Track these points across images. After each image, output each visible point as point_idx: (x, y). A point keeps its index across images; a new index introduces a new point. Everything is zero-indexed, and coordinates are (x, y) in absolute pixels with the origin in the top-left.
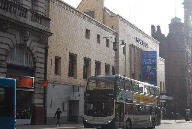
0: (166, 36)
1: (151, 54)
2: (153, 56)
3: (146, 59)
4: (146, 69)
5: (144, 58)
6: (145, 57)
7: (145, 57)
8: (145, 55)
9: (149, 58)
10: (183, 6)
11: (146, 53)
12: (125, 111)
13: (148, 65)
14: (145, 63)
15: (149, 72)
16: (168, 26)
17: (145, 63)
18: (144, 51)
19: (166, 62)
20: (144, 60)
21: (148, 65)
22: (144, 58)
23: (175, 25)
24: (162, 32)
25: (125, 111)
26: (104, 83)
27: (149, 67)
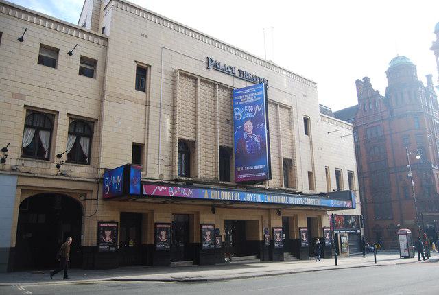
0: (383, 93)
1: (251, 93)
2: (257, 97)
3: (242, 106)
4: (242, 131)
5: (238, 106)
6: (240, 103)
7: (240, 103)
8: (241, 97)
9: (249, 104)
10: (432, 52)
11: (242, 92)
12: (118, 244)
13: (246, 120)
14: (239, 116)
15: (249, 138)
16: (385, 75)
17: (239, 116)
18: (238, 90)
19: (355, 130)
20: (237, 111)
21: (246, 120)
22: (238, 106)
23: (400, 71)
24: (373, 87)
25: (118, 244)
26: (132, 191)
27: (249, 126)
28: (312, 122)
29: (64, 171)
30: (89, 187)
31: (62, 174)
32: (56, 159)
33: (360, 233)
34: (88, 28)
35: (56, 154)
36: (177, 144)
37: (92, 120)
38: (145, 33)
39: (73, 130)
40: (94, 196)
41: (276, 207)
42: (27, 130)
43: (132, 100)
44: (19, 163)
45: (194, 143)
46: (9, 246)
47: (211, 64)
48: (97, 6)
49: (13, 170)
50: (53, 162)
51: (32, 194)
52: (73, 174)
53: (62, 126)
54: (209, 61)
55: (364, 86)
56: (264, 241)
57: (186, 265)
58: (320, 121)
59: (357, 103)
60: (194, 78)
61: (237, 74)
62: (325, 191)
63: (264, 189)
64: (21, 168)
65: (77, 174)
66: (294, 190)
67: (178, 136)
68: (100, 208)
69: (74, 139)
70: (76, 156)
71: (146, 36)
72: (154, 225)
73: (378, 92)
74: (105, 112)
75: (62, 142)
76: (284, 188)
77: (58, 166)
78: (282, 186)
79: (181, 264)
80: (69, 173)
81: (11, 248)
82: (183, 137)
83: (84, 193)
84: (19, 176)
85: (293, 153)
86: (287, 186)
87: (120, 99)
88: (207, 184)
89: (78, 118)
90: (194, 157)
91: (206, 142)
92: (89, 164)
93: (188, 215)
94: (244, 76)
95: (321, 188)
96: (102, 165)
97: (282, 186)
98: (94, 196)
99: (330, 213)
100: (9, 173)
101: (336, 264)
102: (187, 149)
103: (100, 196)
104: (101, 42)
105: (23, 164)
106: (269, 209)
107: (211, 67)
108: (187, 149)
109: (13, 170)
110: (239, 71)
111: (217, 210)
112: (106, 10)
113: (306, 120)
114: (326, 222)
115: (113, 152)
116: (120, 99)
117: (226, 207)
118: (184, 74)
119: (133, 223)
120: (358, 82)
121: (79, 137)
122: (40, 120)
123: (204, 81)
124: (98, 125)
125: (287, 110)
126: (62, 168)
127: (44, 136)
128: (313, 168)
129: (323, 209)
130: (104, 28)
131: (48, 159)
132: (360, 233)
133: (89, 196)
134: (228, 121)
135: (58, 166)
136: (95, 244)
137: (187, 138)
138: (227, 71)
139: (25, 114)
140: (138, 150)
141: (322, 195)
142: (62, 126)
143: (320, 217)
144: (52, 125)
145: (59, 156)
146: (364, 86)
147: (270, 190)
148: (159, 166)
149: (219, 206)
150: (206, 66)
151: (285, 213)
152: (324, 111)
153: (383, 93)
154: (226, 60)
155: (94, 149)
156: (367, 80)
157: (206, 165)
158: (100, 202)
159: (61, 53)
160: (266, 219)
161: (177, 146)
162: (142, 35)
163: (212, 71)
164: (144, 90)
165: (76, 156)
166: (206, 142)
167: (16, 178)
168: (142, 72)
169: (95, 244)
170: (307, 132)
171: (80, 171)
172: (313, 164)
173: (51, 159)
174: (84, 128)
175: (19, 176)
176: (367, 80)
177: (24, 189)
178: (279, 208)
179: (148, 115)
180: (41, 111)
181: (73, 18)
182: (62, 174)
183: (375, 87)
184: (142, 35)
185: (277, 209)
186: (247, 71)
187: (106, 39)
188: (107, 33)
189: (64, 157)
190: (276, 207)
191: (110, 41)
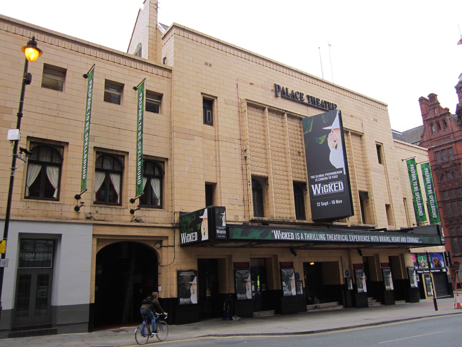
16: (455, 90)
28: (385, 150)
29: (139, 217)
30: (164, 233)
31: (137, 221)
32: (130, 204)
33: (446, 273)
34: (145, 56)
35: (129, 199)
36: (251, 181)
37: (162, 160)
38: (209, 62)
39: (101, 166)
40: (170, 242)
41: (356, 246)
42: (31, 166)
43: (202, 135)
44: (93, 210)
45: (266, 179)
46: (88, 302)
47: (280, 92)
48: (153, 34)
49: (88, 218)
50: (127, 208)
51: (108, 244)
52: (148, 219)
53: (132, 167)
54: (277, 88)
55: (429, 104)
56: (346, 285)
57: (267, 315)
58: (394, 148)
59: (421, 123)
60: (260, 107)
61: (306, 101)
62: (406, 226)
63: (346, 227)
64: (95, 216)
65: (151, 220)
66: (374, 226)
67: (250, 173)
68: (177, 255)
69: (102, 177)
70: (147, 200)
71: (210, 65)
72: (242, 271)
73: (447, 110)
74: (175, 151)
75: (131, 181)
76: (362, 225)
77: (132, 212)
78: (360, 222)
79: (262, 314)
80: (144, 219)
81: (91, 305)
82: (255, 173)
83: (160, 240)
84: (94, 224)
85: (368, 185)
86: (364, 222)
87: (189, 135)
88: (283, 225)
89: (148, 158)
90: (267, 194)
91: (278, 177)
92: (161, 207)
93: (265, 259)
94: (313, 102)
95: (400, 222)
96: (177, 209)
97: (360, 222)
98: (170, 242)
99: (413, 250)
100: (84, 221)
101: (436, 309)
102: (259, 185)
103: (177, 242)
104: (166, 74)
105: (97, 212)
106: (348, 249)
107: (279, 95)
108: (259, 185)
109: (88, 218)
110: (308, 96)
111: (298, 252)
112: (165, 40)
113: (379, 147)
114: (410, 262)
115: (185, 196)
116: (189, 135)
117: (305, 248)
118: (251, 105)
119: (208, 271)
120: (422, 100)
121: (108, 173)
122: (45, 153)
123: (273, 110)
124: (169, 164)
125: (359, 138)
126: (136, 213)
127: (115, 179)
128: (391, 200)
129: (407, 246)
130: (165, 58)
131: (120, 205)
132: (446, 273)
133: (165, 243)
134: (299, 152)
135: (132, 212)
136: (175, 295)
137: (259, 174)
138: (295, 98)
139: (95, 156)
140: (210, 189)
141: (404, 232)
142: (132, 167)
143: (402, 256)
144: (62, 159)
145: (132, 201)
146: (429, 104)
147: (353, 227)
148: (236, 208)
149: (299, 248)
150: (274, 94)
151: (367, 253)
152: (396, 135)
153: (453, 111)
154: (292, 86)
155: (166, 191)
156: (433, 97)
157: (281, 205)
158: (177, 249)
159: (125, 88)
160: (345, 259)
161: (251, 183)
162: (206, 64)
163: (280, 99)
164: (211, 124)
165: (147, 200)
166: (278, 177)
167: (91, 227)
168: (209, 103)
169: (175, 295)
170: (380, 162)
171: (153, 216)
172: (390, 196)
173: (124, 204)
174: (154, 167)
175: (94, 224)
176: (433, 97)
177: (99, 238)
178: (359, 247)
179: (219, 151)
180: (111, 152)
181: (123, 49)
182: (137, 221)
183: (443, 105)
184: (206, 64)
185: (356, 248)
186: (316, 97)
187: (170, 71)
188: (170, 64)
189: (137, 202)
190: (356, 246)
191: (174, 72)
